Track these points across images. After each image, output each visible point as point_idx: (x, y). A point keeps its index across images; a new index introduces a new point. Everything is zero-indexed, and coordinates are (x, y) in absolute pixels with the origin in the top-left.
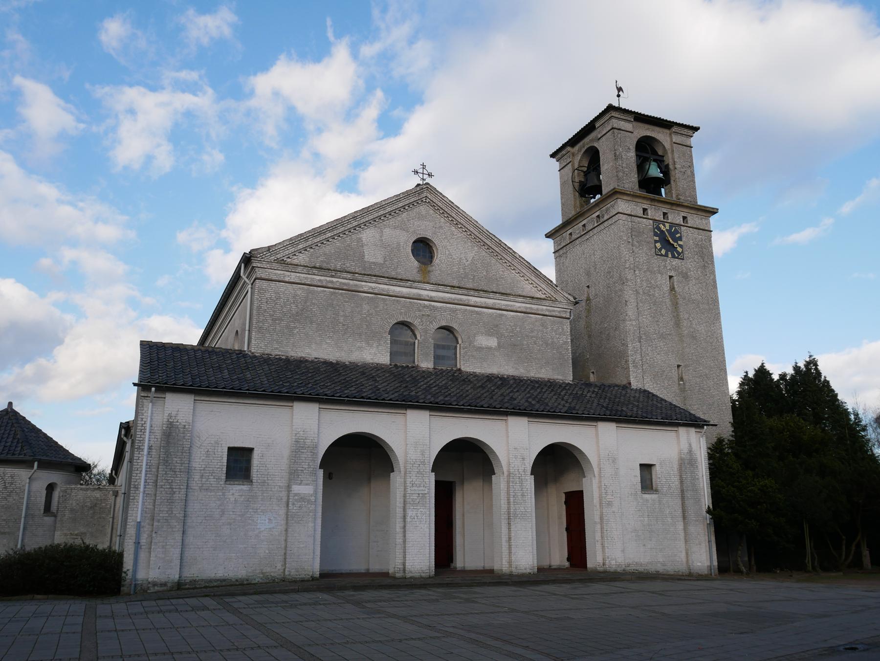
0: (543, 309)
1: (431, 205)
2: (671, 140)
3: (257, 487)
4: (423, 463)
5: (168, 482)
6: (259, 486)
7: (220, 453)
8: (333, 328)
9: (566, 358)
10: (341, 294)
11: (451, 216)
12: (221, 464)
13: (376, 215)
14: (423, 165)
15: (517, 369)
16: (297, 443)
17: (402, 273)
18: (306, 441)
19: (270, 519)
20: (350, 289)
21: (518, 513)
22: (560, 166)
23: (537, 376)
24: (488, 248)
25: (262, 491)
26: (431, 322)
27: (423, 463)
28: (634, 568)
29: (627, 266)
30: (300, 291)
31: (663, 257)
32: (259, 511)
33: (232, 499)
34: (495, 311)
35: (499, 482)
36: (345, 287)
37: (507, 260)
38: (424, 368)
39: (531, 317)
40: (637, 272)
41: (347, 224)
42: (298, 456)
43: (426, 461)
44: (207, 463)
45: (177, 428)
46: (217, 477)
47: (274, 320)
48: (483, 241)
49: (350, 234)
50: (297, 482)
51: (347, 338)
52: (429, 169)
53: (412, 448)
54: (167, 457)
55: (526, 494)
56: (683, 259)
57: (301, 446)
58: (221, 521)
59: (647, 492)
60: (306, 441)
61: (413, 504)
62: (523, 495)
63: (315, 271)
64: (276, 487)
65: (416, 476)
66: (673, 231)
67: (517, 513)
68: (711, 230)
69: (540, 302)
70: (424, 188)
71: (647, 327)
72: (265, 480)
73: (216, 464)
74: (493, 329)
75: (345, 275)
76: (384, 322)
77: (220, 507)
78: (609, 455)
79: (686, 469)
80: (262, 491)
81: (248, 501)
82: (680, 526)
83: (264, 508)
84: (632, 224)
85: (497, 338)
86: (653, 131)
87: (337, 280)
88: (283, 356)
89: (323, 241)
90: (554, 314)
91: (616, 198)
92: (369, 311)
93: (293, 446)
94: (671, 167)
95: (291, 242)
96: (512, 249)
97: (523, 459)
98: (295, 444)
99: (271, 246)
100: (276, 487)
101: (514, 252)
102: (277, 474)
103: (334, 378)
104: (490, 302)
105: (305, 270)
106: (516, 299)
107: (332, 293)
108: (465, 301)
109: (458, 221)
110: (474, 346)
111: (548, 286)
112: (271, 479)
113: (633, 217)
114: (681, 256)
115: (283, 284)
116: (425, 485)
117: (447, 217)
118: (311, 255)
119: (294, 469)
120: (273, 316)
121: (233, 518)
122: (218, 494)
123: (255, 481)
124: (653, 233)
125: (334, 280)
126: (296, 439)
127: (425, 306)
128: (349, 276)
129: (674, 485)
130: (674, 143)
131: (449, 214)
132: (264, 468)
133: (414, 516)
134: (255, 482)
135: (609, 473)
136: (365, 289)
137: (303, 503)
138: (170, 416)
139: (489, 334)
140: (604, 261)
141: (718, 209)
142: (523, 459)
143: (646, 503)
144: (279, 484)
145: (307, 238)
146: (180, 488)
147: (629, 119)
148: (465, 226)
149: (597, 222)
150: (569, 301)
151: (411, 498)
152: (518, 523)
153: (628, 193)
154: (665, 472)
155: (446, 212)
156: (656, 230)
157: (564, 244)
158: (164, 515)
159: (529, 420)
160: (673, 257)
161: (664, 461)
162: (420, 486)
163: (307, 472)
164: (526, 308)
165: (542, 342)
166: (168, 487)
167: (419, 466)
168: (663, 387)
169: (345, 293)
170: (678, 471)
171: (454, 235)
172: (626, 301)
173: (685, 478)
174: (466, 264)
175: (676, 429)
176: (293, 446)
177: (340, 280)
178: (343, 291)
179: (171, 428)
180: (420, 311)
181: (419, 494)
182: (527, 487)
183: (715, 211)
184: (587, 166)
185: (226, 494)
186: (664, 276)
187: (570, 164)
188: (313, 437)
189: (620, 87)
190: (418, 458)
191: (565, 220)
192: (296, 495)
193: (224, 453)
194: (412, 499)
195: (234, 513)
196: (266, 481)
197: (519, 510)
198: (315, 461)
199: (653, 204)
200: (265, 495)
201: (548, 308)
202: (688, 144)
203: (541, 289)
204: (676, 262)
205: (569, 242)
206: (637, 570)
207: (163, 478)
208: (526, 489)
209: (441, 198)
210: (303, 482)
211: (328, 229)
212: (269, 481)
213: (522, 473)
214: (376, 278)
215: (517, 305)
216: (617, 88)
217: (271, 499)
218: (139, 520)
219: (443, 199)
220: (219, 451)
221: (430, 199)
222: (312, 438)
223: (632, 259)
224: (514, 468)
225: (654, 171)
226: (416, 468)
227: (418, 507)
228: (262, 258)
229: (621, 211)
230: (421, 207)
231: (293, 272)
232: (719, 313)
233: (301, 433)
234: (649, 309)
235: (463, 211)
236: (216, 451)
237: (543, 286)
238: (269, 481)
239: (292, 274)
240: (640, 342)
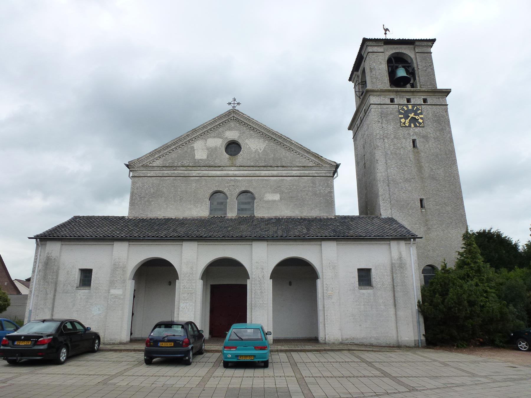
1: (237, 121)
3: (93, 291)
4: (191, 274)
5: (44, 289)
6: (94, 290)
7: (74, 272)
8: (174, 199)
9: (330, 202)
10: (179, 180)
11: (249, 125)
12: (74, 278)
13: (202, 132)
14: (234, 99)
15: (293, 212)
16: (114, 265)
17: (218, 162)
18: (119, 264)
19: (99, 309)
20: (185, 176)
21: (258, 304)
23: (308, 215)
24: (274, 141)
25: (95, 292)
26: (235, 189)
27: (191, 274)
28: (351, 341)
29: (378, 137)
30: (155, 181)
31: (407, 128)
32: (93, 304)
33: (79, 297)
34: (278, 177)
35: (180, 285)
36: (182, 175)
37: (287, 146)
38: (229, 217)
39: (304, 179)
40: (386, 140)
41: (183, 140)
42: (115, 272)
43: (194, 273)
44: (67, 278)
45: (51, 259)
46: (72, 286)
47: (141, 198)
48: (271, 137)
49: (187, 145)
50: (113, 287)
51: (182, 204)
52: (238, 100)
53: (185, 265)
54: (45, 275)
55: (264, 292)
57: (117, 266)
58: (73, 310)
59: (363, 288)
60: (119, 264)
61: (184, 299)
62: (261, 292)
63: (164, 169)
64: (103, 290)
65: (187, 282)
66: (415, 109)
67: (257, 304)
68: (447, 104)
70: (232, 112)
71: (394, 175)
72: (97, 287)
73: (72, 278)
74: (276, 189)
75: (182, 168)
76: (205, 192)
77: (73, 302)
78: (330, 264)
79: (396, 270)
80: (95, 292)
81: (88, 298)
82: (392, 311)
83: (96, 302)
85: (280, 194)
86: (401, 48)
87: (177, 172)
88: (145, 217)
89: (170, 152)
90: (321, 175)
91: (369, 95)
92: (196, 187)
93: (112, 267)
94: (416, 69)
95: (150, 154)
96: (289, 138)
97: (263, 269)
98: (113, 266)
99: (139, 158)
100: (103, 290)
101: (291, 140)
102: (104, 283)
103: (350, 226)
104: (275, 173)
105: (158, 169)
106: (293, 169)
107: (174, 180)
108: (257, 174)
109: (254, 127)
110: (264, 201)
112: (101, 286)
113: (382, 105)
115: (147, 178)
116: (192, 288)
117: (247, 126)
118: (164, 160)
119: (112, 280)
120: (140, 196)
121: (79, 308)
122: (72, 295)
123: (92, 287)
124: (398, 113)
125: (176, 172)
126: (114, 263)
127: (231, 180)
128: (184, 169)
129: (387, 282)
130: (417, 53)
131: (248, 124)
132: (98, 280)
133: (184, 307)
134: (92, 288)
135: (330, 276)
136: (194, 175)
137: (116, 299)
138: (48, 253)
139: (274, 192)
141: (451, 89)
142: (263, 269)
143: (362, 296)
144: (105, 289)
145: (160, 151)
146: (51, 292)
147: (380, 44)
148: (258, 130)
150: (331, 166)
151: (183, 295)
152: (257, 311)
153: (377, 90)
154: (379, 273)
155: (246, 123)
158: (42, 306)
159: (406, 243)
160: (415, 126)
161: (378, 265)
162: (189, 288)
163: (119, 281)
164: (301, 173)
165: (312, 193)
166: (45, 291)
167: (189, 276)
168: (408, 214)
169: (182, 179)
170: (390, 272)
171: (252, 136)
172: (377, 160)
173: (396, 277)
174: (260, 152)
175: (181, 243)
176: (112, 267)
177: (179, 172)
178: (181, 178)
179: (48, 260)
180: (228, 183)
181: (188, 293)
182: (264, 287)
183: (449, 90)
185: (76, 295)
186: (408, 140)
188: (124, 261)
189: (387, 29)
190: (189, 271)
192: (112, 295)
193: (76, 272)
194: (183, 296)
195: (80, 305)
196: (98, 287)
197: (259, 303)
198: (124, 275)
199: (397, 94)
200: (97, 295)
201: (317, 171)
202: (428, 51)
204: (417, 130)
206: (353, 343)
207: (43, 286)
208: (264, 289)
209: (242, 115)
210: (117, 287)
211: (172, 144)
212: (100, 287)
213: (262, 278)
214: (200, 167)
215: (294, 173)
216: (384, 29)
217: (100, 297)
218: (30, 309)
219: (243, 116)
220: (74, 271)
221: (236, 117)
222: (123, 262)
223: (381, 132)
224: (255, 275)
225: (401, 73)
227: (188, 301)
228: (135, 165)
230: (231, 123)
231: (152, 171)
232: (456, 159)
233: (117, 259)
235: (256, 121)
236: (72, 271)
238: (100, 287)
239: (152, 172)
240: (388, 186)
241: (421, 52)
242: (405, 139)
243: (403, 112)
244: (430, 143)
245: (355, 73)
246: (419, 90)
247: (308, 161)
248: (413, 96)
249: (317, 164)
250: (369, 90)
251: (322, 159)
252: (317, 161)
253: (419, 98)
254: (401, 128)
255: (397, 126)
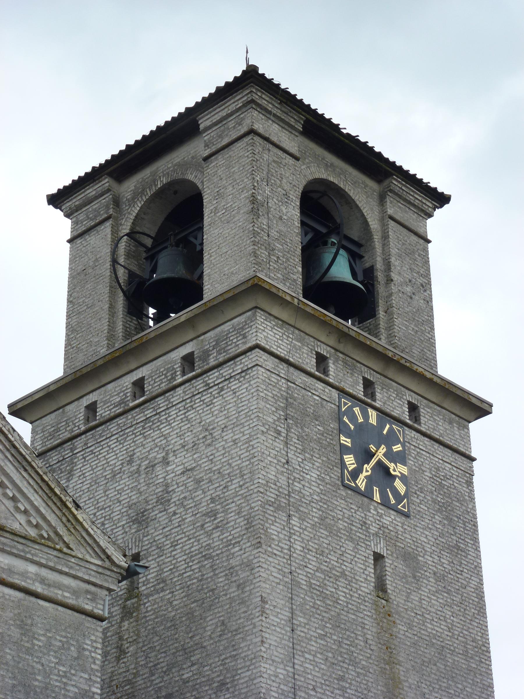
0: (27, 572)
2: (383, 211)
22: (73, 230)
40: (295, 521)
56: (407, 515)
66: (385, 432)
69: (20, 547)
71: (314, 689)
84: (288, 388)
94: (380, 276)
111: (50, 503)
113: (292, 369)
114: (404, 506)
139: (325, 530)
140: (198, 481)
147: (292, 122)
149: (184, 373)
150: (107, 564)
153: (288, 298)
156: (345, 419)
157: (67, 435)
165: (14, 678)
183: (485, 407)
184: (153, 235)
187: (108, 224)
191: (70, 372)
199: (341, 347)
201: (44, 572)
203: (28, 507)
205: (83, 428)
223: (283, 481)
226: (457, 535)
229: (263, 344)
234: (322, 637)
237: (37, 501)
241: (402, 220)
242: (352, 540)
243: (352, 427)
244: (425, 592)
245: (106, 182)
246: (408, 365)
247: (10, 504)
248: (383, 378)
249: (46, 535)
250: (263, 285)
251: (80, 517)
252: (51, 518)
253: (399, 396)
254: (343, 492)
255: (331, 477)
